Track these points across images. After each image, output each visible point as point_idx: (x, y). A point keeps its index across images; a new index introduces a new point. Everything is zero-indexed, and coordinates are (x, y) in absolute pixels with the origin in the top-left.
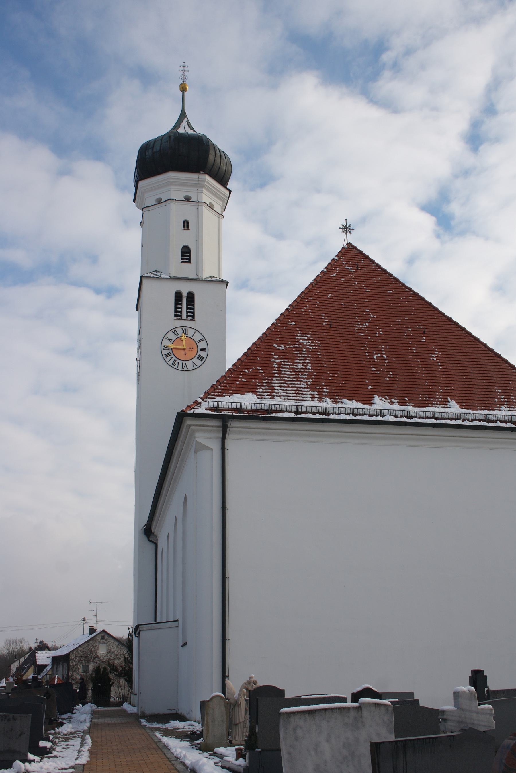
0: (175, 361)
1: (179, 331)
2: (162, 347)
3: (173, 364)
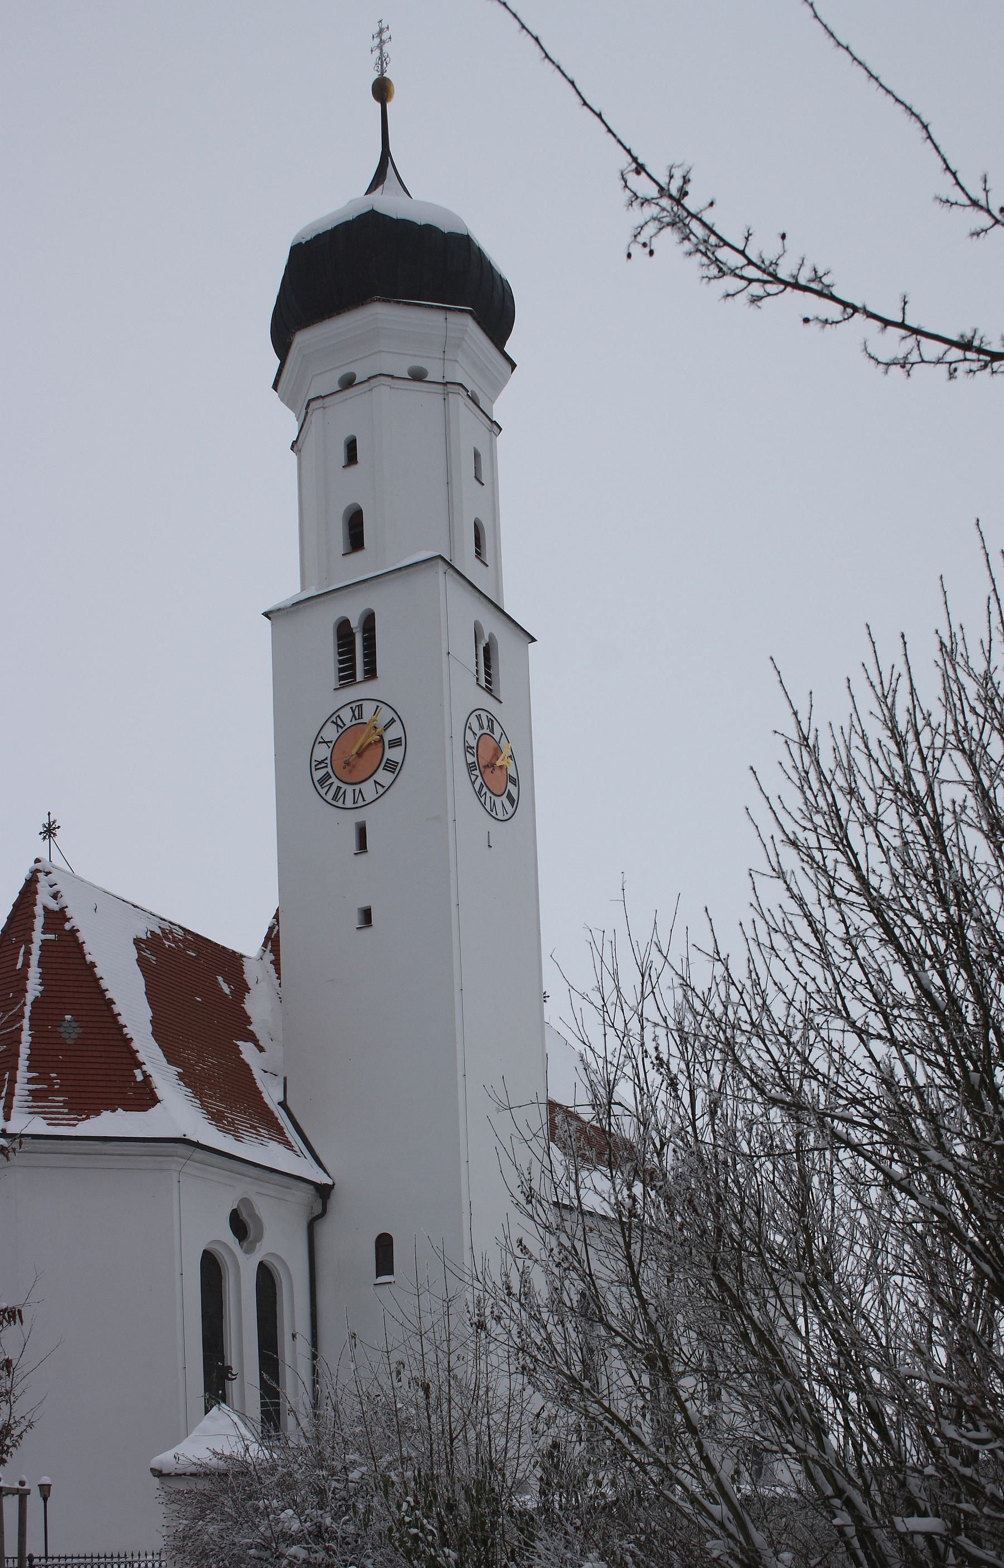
0: (339, 788)
2: (314, 763)
3: (335, 798)
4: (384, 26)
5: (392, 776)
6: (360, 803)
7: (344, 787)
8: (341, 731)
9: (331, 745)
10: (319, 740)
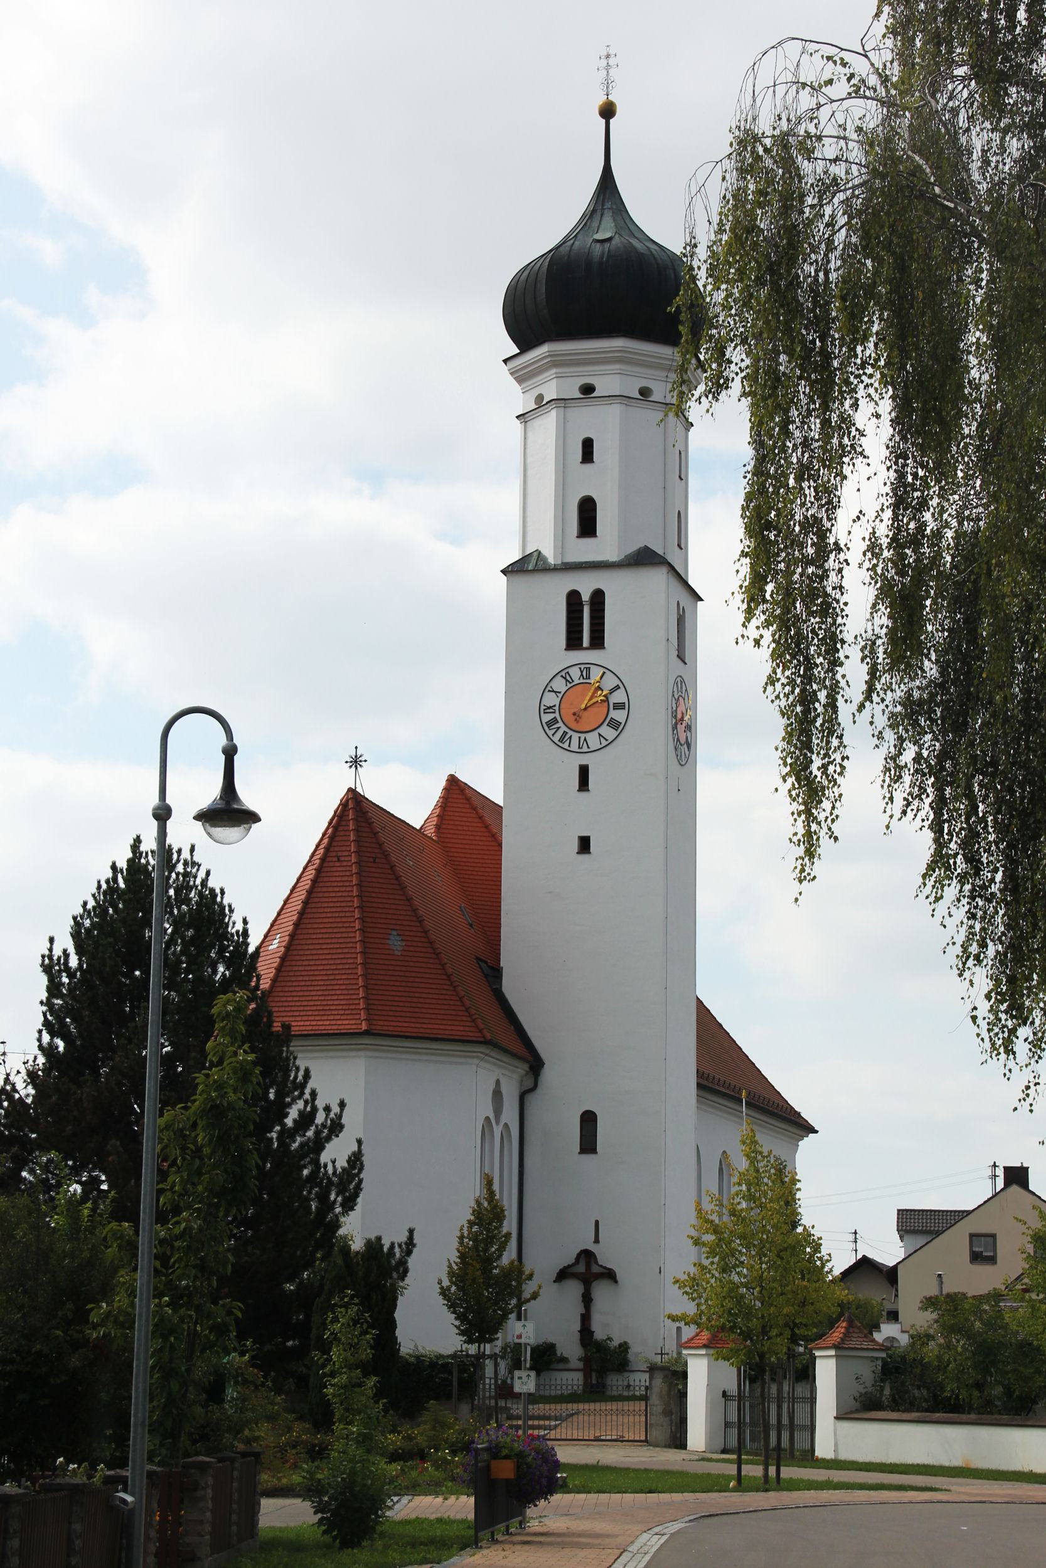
0: (565, 733)
1: (575, 673)
2: (543, 708)
3: (561, 740)
4: (612, 52)
5: (616, 733)
6: (585, 749)
7: (570, 733)
8: (569, 685)
9: (560, 696)
10: (548, 689)
